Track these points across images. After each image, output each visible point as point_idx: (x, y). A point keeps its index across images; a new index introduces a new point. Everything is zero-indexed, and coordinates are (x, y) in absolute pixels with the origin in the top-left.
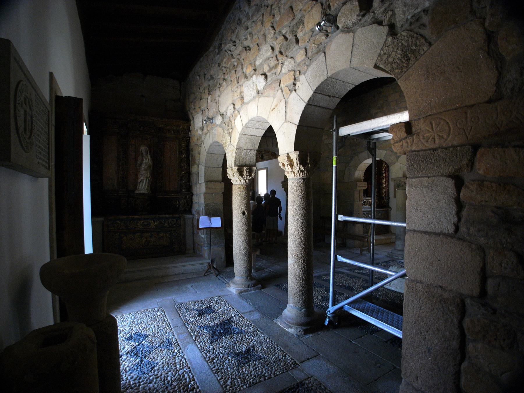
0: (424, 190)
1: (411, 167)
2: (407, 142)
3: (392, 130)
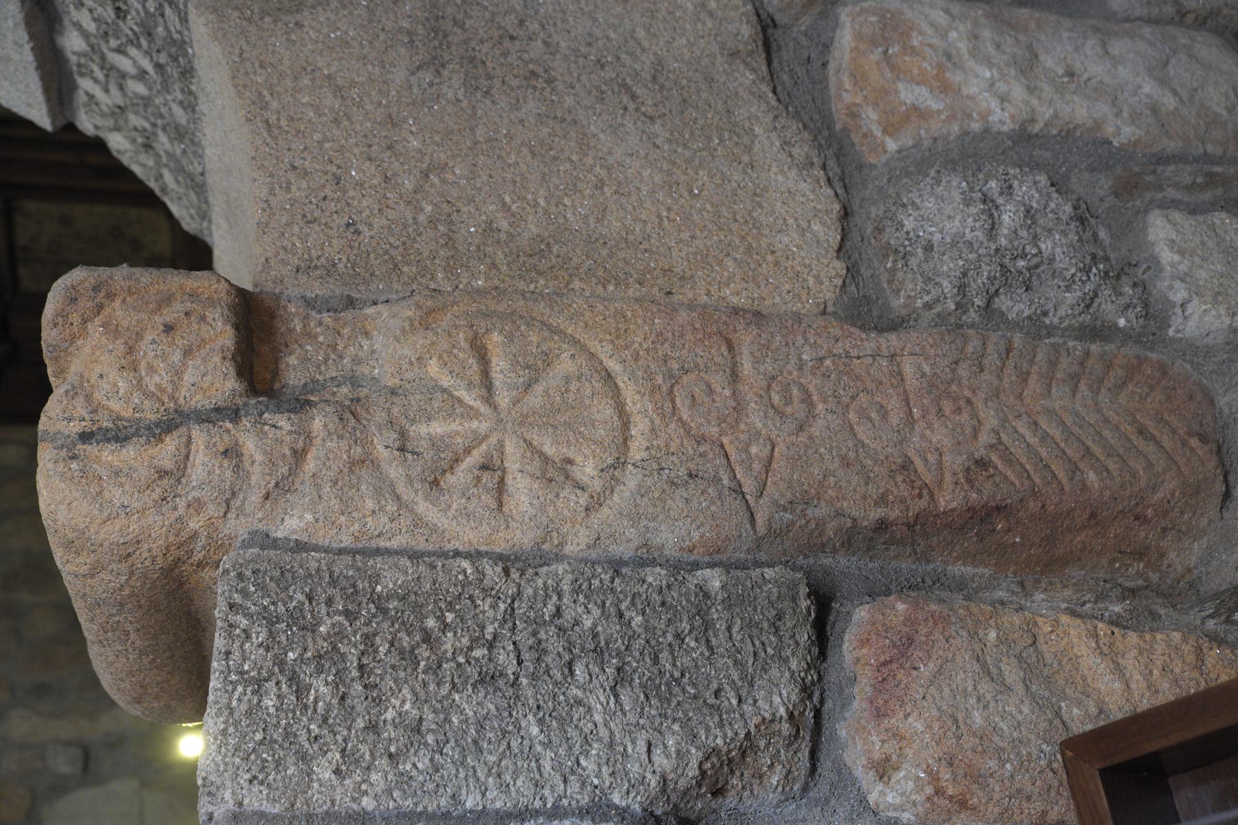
1: (270, 702)
2: (232, 453)
3: (85, 304)
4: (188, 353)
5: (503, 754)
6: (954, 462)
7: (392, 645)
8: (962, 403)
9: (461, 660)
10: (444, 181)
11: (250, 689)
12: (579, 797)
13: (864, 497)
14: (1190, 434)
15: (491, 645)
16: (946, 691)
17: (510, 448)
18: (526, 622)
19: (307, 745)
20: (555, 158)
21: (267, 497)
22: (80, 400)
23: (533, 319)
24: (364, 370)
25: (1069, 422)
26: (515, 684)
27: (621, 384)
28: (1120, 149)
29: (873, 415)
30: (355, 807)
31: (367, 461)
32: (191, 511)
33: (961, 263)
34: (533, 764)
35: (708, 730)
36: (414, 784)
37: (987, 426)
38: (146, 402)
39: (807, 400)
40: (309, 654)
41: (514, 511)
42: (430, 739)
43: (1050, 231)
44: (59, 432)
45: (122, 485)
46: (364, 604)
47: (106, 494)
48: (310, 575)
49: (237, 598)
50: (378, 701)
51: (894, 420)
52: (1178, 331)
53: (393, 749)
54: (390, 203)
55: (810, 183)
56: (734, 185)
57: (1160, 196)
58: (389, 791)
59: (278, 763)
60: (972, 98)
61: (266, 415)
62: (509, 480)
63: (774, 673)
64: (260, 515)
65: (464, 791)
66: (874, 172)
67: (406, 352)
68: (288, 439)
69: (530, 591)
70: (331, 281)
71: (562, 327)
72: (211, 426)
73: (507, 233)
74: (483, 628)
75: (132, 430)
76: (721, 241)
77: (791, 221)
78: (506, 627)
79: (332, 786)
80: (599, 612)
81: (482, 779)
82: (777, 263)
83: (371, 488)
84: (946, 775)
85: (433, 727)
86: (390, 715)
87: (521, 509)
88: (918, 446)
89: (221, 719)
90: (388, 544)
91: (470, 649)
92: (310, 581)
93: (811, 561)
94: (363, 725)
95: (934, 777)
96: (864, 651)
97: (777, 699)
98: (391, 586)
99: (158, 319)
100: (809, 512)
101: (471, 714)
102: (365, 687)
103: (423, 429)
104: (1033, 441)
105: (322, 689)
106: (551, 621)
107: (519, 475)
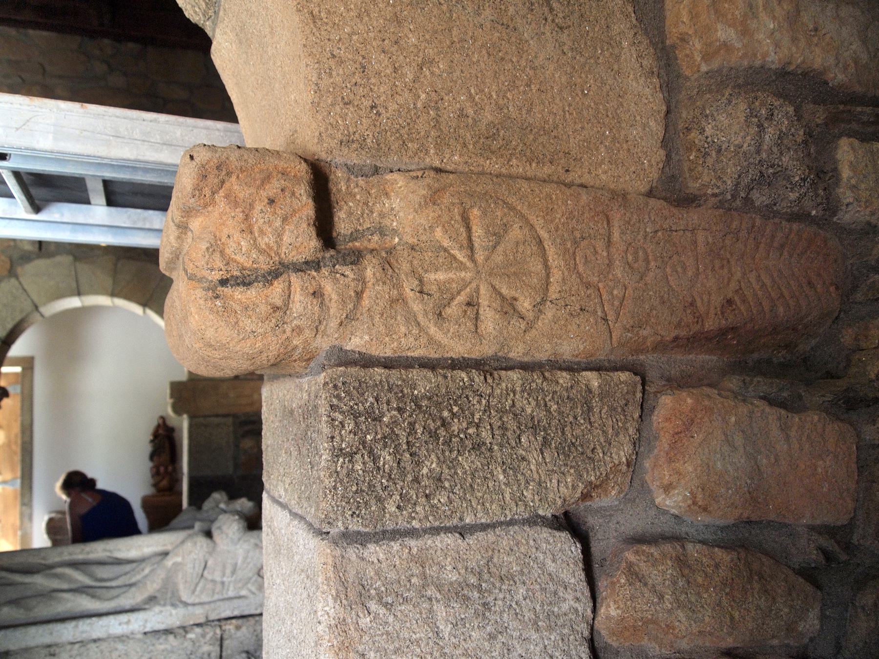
0: (440, 611)
1: (358, 467)
2: (317, 294)
3: (213, 180)
4: (285, 220)
5: (485, 492)
6: (717, 300)
7: (424, 428)
8: (725, 262)
9: (462, 436)
10: (432, 73)
11: (347, 459)
12: (523, 514)
13: (669, 323)
14: (831, 284)
15: (478, 426)
16: (707, 450)
17: (483, 291)
18: (497, 411)
19: (382, 493)
20: (502, 59)
21: (341, 324)
22: (217, 256)
23: (498, 199)
24: (386, 222)
25: (775, 275)
26: (491, 450)
27: (546, 246)
28: (832, 88)
29: (679, 269)
30: (408, 526)
31: (400, 300)
32: (295, 334)
33: (739, 168)
34: (501, 496)
35: (588, 472)
36: (439, 512)
37: (735, 278)
38: (260, 257)
39: (647, 261)
40: (379, 436)
41: (484, 332)
42: (447, 484)
43: (789, 149)
44: (204, 277)
45: (250, 317)
46: (408, 403)
47: (241, 324)
48: (376, 384)
49: (335, 401)
50: (418, 464)
51: (690, 274)
52: (838, 219)
53: (427, 492)
54: (399, 90)
55: (651, 89)
56: (608, 87)
57: (848, 127)
58: (427, 517)
59: (366, 503)
60: (759, 42)
61: (337, 266)
62: (481, 312)
63: (621, 436)
64: (336, 336)
65: (465, 514)
66: (688, 84)
67: (422, 221)
68: (352, 284)
69: (499, 391)
70: (364, 153)
71: (514, 204)
72: (303, 274)
73: (472, 119)
74: (473, 415)
75: (254, 277)
76: (598, 132)
77: (638, 118)
78: (486, 414)
79: (396, 516)
80: (535, 403)
81: (475, 507)
82: (629, 150)
83: (403, 319)
84: (700, 496)
85: (449, 477)
86: (425, 471)
87: (488, 331)
88: (699, 289)
89: (333, 479)
90: (412, 354)
91: (467, 429)
92: (376, 389)
93: (635, 357)
94: (411, 479)
95: (694, 496)
96: (667, 424)
97: (622, 453)
98: (423, 391)
99: (264, 194)
100: (640, 332)
101: (468, 468)
102: (411, 455)
103: (432, 276)
104: (757, 287)
105: (387, 457)
106: (510, 410)
107: (488, 309)
